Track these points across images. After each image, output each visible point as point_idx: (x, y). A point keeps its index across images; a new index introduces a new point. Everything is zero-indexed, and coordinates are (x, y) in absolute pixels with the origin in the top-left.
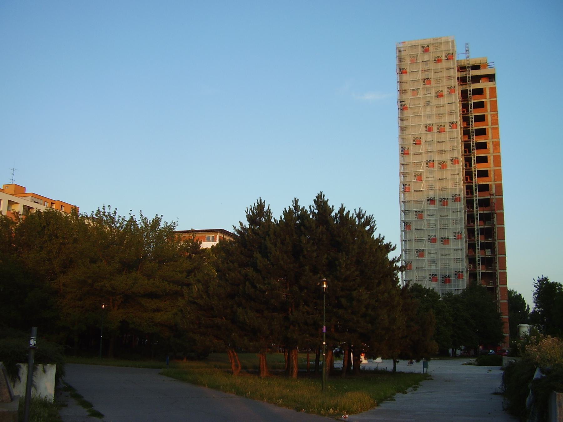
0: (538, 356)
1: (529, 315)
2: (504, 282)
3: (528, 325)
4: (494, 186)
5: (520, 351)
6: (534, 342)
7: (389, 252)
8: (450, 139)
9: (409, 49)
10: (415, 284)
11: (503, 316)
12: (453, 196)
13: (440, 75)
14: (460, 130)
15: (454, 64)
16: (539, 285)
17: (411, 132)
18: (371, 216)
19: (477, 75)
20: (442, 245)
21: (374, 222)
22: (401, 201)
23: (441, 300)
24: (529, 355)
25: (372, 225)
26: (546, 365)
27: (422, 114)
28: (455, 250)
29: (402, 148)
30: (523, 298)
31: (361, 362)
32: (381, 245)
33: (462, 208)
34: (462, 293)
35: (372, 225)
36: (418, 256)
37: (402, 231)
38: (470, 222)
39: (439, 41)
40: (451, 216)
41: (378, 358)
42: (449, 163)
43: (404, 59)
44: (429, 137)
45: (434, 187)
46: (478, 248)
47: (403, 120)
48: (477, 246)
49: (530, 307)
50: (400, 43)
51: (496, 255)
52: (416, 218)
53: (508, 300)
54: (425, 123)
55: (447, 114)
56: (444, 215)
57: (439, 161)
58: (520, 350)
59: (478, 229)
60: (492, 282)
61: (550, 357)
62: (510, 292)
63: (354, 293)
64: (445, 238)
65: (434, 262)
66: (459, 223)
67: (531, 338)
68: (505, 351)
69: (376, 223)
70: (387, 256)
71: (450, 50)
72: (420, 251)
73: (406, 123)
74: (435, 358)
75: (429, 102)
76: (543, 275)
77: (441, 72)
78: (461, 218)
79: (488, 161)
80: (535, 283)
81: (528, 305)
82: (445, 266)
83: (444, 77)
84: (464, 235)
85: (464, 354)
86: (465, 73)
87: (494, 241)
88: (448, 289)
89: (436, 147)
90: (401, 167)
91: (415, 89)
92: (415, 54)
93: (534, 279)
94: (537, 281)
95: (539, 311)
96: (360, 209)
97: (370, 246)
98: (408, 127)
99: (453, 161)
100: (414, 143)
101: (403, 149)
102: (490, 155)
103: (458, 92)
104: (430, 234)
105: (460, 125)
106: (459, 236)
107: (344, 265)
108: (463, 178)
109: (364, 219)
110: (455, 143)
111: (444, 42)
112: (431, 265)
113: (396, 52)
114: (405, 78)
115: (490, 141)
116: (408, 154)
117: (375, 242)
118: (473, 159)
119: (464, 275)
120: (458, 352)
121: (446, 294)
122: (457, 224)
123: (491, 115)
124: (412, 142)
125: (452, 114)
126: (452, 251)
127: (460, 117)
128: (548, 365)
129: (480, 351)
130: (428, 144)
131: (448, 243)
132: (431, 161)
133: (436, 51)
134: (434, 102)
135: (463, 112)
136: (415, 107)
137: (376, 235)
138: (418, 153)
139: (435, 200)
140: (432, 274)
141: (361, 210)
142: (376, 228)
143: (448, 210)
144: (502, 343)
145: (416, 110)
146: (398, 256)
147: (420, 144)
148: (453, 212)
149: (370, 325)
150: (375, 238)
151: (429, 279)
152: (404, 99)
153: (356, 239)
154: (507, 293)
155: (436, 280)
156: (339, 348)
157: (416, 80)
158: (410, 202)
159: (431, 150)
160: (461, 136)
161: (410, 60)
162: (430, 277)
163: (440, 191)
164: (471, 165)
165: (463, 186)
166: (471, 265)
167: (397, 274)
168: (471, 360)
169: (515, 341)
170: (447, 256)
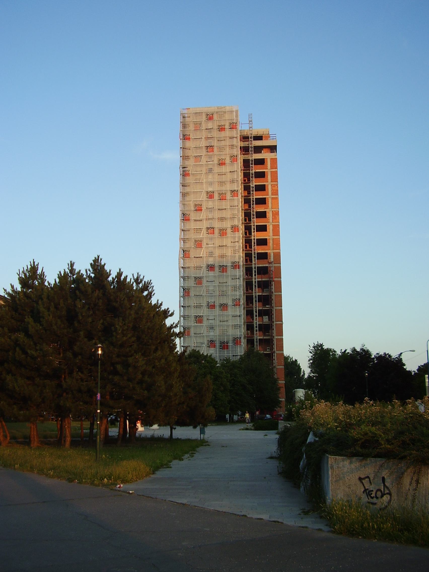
0: (311, 420)
2: (281, 348)
3: (303, 390)
4: (273, 254)
7: (166, 317)
10: (193, 350)
11: (279, 382)
12: (233, 263)
13: (223, 143)
15: (237, 134)
16: (314, 351)
18: (149, 281)
20: (220, 311)
21: (152, 287)
23: (219, 366)
24: (303, 419)
25: (150, 290)
27: (204, 181)
30: (299, 364)
31: (137, 429)
32: (158, 310)
35: (150, 290)
36: (196, 322)
37: (180, 297)
39: (223, 110)
40: (230, 283)
42: (229, 231)
43: (187, 125)
44: (210, 204)
46: (256, 315)
47: (184, 186)
48: (254, 312)
50: (184, 109)
51: (273, 322)
52: (195, 284)
53: (284, 366)
54: (207, 190)
56: (223, 282)
58: (295, 415)
59: (256, 296)
61: (323, 421)
62: (286, 358)
63: (130, 360)
64: (224, 304)
65: (212, 328)
66: (237, 290)
67: (306, 403)
68: (281, 416)
70: (165, 322)
71: (234, 120)
72: (199, 317)
73: (187, 189)
74: (213, 424)
75: (211, 170)
76: (318, 342)
77: (225, 140)
79: (267, 230)
82: (223, 332)
83: (226, 146)
84: (242, 302)
85: (241, 419)
86: (247, 143)
87: (272, 308)
88: (226, 355)
89: (217, 215)
90: (181, 233)
91: (198, 156)
93: (309, 346)
94: (313, 347)
95: (314, 376)
96: (138, 274)
97: (148, 311)
99: (233, 228)
100: (195, 209)
101: (184, 214)
105: (241, 193)
106: (238, 303)
108: (242, 246)
109: (142, 284)
111: (228, 111)
114: (188, 144)
115: (270, 211)
116: (188, 220)
118: (252, 227)
119: (241, 341)
121: (224, 360)
123: (272, 185)
124: (193, 209)
126: (230, 317)
127: (241, 185)
128: (321, 429)
130: (209, 211)
131: (227, 310)
132: (211, 228)
133: (219, 119)
134: (217, 169)
135: (245, 180)
136: (197, 173)
137: (154, 301)
138: (198, 220)
141: (139, 275)
143: (227, 277)
144: (278, 408)
145: (198, 177)
147: (201, 210)
149: (146, 392)
150: (153, 303)
153: (133, 304)
155: (215, 346)
157: (199, 147)
158: (189, 268)
164: (250, 234)
166: (249, 331)
167: (175, 340)
168: (247, 425)
169: (291, 406)
170: (225, 322)
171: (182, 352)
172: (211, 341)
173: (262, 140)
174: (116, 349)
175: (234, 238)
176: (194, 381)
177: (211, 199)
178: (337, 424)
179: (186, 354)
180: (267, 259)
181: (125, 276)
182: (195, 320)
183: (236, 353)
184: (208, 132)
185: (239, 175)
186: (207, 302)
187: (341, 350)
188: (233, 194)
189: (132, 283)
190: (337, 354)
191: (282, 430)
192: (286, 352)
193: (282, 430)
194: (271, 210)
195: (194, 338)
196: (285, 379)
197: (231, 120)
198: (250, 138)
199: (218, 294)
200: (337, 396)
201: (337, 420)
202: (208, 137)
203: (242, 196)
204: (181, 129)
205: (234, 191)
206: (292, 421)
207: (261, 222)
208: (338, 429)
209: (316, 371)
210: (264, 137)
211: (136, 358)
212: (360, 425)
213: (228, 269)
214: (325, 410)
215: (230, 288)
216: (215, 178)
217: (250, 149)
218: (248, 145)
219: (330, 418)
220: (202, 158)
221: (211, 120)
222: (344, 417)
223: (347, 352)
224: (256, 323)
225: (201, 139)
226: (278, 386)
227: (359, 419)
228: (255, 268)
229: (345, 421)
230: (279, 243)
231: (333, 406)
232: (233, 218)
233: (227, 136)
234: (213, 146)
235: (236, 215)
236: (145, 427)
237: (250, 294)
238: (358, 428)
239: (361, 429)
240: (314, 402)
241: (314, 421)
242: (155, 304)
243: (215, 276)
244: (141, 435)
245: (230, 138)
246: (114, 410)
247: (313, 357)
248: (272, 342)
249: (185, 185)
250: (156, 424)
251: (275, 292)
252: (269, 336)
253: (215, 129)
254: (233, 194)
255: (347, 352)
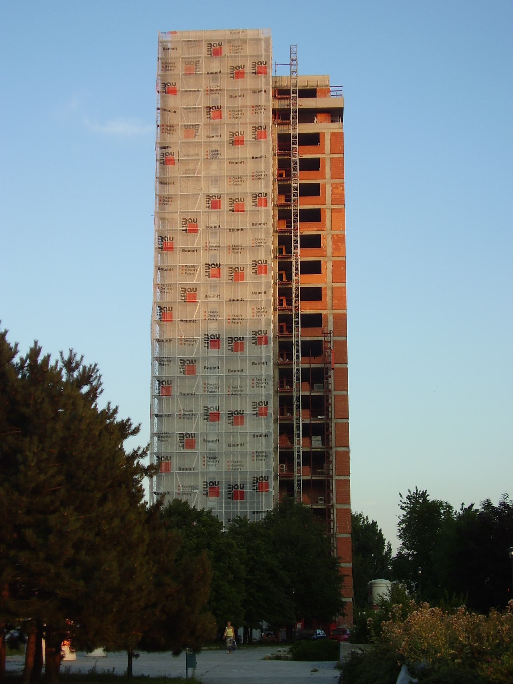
0: (403, 643)
1: (390, 563)
2: (346, 498)
3: (388, 582)
4: (332, 317)
5: (373, 632)
6: (397, 615)
7: (125, 436)
8: (253, 224)
9: (183, 46)
10: (176, 500)
11: (343, 565)
12: (255, 333)
13: (240, 102)
14: (273, 210)
15: (267, 84)
16: (409, 505)
17: (179, 208)
18: (93, 367)
19: (310, 107)
20: (230, 425)
21: (98, 378)
22: (154, 339)
23: (225, 532)
24: (387, 640)
25: (94, 383)
26: (420, 661)
27: (203, 174)
28: (254, 436)
29: (160, 238)
30: (380, 530)
31: (63, 657)
32: (110, 423)
33: (270, 357)
34: (265, 519)
35: (94, 383)
36: (183, 446)
37: (153, 397)
38: (285, 384)
39: (241, 36)
40: (249, 371)
41: (97, 649)
42: (249, 271)
43: (171, 65)
44: (214, 219)
45: (218, 314)
46: (297, 434)
47: (164, 184)
48: (295, 429)
49: (392, 547)
50: (165, 33)
51: (331, 448)
52: (181, 372)
53: (351, 534)
54: (206, 192)
55: (248, 178)
56: (236, 369)
57: (230, 266)
58: (373, 631)
59: (298, 398)
60: (323, 498)
61: (426, 645)
62: (356, 519)
63: (53, 519)
64: (236, 412)
65: (213, 457)
66: (263, 385)
67: (393, 608)
68: (344, 631)
69: (102, 380)
70: (122, 446)
71: (261, 56)
72: (187, 436)
73: (170, 190)
74: (211, 647)
75: (216, 153)
76: (416, 487)
77: (243, 96)
78: (268, 376)
79: (322, 271)
80: (403, 501)
81: (389, 543)
82: (235, 466)
83: (246, 107)
84: (271, 409)
85: (266, 638)
86: (286, 102)
87: (328, 421)
88: (239, 510)
89: (226, 240)
90: (156, 274)
91: (191, 125)
92: (194, 58)
93: (400, 494)
94: (407, 498)
95: (409, 555)
96: (71, 351)
97: (88, 425)
98: (174, 197)
99: (257, 267)
100: (185, 229)
101: (162, 238)
102: (326, 259)
103: (273, 138)
104: (208, 403)
105: (273, 200)
106: (264, 410)
107: (35, 461)
108: (274, 300)
109: (79, 371)
110: (261, 233)
111: (250, 40)
112: (207, 465)
113: (157, 50)
114: (173, 101)
116: (171, 249)
117: (98, 418)
118: (294, 265)
119: (269, 483)
120: (256, 634)
121: (234, 520)
122: (259, 387)
123: (332, 185)
124: (179, 227)
125: (258, 179)
126: (248, 438)
127: (273, 184)
128: (423, 660)
129: (298, 632)
130: (211, 233)
131: (242, 423)
132: (215, 265)
133: (234, 54)
134: (227, 153)
135: (280, 175)
136: (190, 160)
137: (101, 404)
138: (190, 249)
139: (219, 340)
140: (208, 482)
141: (73, 354)
142: (102, 390)
143: (243, 360)
144: (340, 616)
145: (191, 167)
146: (144, 445)
147: (196, 231)
148: (253, 363)
149: (82, 583)
150: (100, 408)
151: (204, 490)
152: (170, 143)
153: (60, 410)
154: (350, 521)
155: (217, 494)
156: (18, 630)
157: (193, 108)
158: (171, 341)
159: (216, 245)
160: (274, 221)
161: (184, 68)
162: (205, 486)
163: (229, 323)
164: (289, 277)
165: (274, 315)
166: (284, 465)
167: (140, 481)
168: (279, 649)
169: (364, 613)
170: (239, 447)
171: (153, 504)
172: (211, 484)
173: (316, 97)
174: (24, 499)
175: (259, 284)
176: (176, 561)
177: (215, 210)
178: (453, 652)
179: (162, 509)
180: (322, 327)
181: (46, 355)
182: (181, 442)
183: (258, 507)
184: (211, 79)
185: (269, 164)
186: (204, 407)
187: (463, 504)
188: (257, 200)
189: (58, 369)
190: (454, 511)
191: (346, 660)
192: (356, 507)
193: (347, 662)
194: (329, 232)
195: (179, 401)
196: (353, 558)
197: (257, 56)
198: (291, 92)
199: (225, 392)
200: (455, 594)
201: (454, 643)
202: (211, 89)
203: (274, 205)
204: (160, 73)
205: (260, 195)
206: (366, 644)
207: (310, 256)
208: (456, 661)
209: (413, 544)
210: (318, 92)
211: (64, 515)
212: (500, 655)
213: (246, 345)
214: (431, 622)
215: (248, 381)
216: (224, 170)
217: (292, 114)
218: (288, 105)
219: (442, 639)
220: (200, 129)
221: (218, 57)
222: (468, 638)
223: (474, 508)
224: (298, 450)
225: (197, 93)
226: (339, 574)
227: (497, 641)
228: (298, 344)
229: (469, 645)
230: (344, 295)
231: (446, 615)
232: (257, 247)
233: (248, 87)
234: (221, 106)
235: (262, 241)
236: (79, 653)
237: (288, 394)
238: (496, 660)
239: (503, 663)
240: (408, 606)
241: (410, 645)
242: (103, 411)
243: (219, 359)
244: (69, 670)
245: (253, 92)
246: (18, 619)
247: (408, 518)
248: (329, 487)
249: (165, 182)
250: (100, 647)
251: (334, 391)
252: (322, 474)
253: (224, 74)
254: (257, 200)
255: (474, 508)
